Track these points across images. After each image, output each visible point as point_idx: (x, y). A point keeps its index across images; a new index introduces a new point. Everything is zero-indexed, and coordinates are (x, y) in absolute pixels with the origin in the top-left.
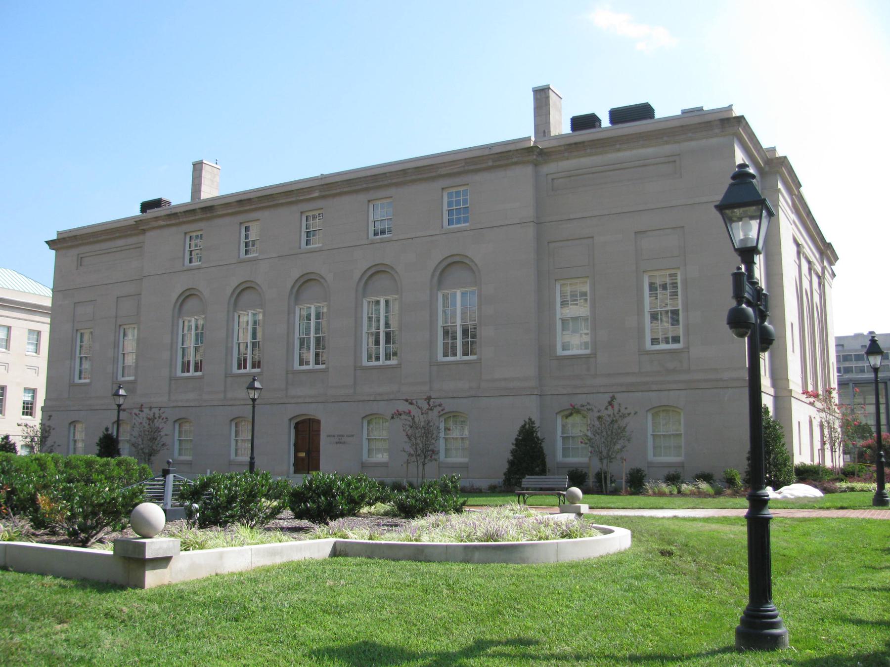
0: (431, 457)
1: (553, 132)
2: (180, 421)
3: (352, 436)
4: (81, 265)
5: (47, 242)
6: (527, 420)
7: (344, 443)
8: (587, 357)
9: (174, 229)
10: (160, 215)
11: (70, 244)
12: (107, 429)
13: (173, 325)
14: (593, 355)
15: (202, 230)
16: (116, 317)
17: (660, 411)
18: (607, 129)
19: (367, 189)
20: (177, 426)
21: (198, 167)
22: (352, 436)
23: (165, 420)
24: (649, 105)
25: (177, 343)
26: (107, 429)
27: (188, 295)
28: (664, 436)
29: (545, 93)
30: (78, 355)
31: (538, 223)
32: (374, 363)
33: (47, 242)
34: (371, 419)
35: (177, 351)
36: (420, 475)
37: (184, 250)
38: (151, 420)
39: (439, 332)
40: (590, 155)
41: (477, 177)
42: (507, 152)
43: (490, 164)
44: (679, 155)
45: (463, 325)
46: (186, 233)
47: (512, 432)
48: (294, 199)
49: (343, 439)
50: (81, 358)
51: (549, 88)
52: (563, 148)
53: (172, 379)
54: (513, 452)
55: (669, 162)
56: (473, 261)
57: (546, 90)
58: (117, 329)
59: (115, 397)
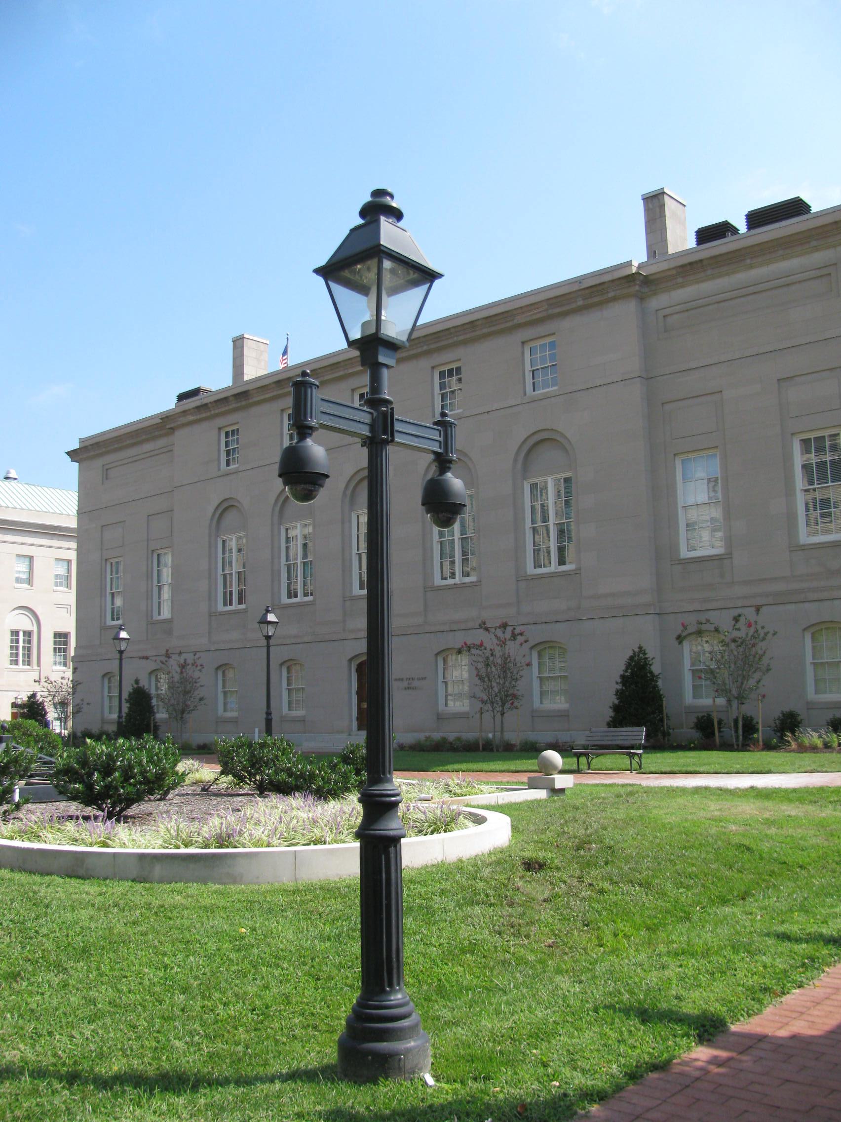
0: (512, 704)
1: (672, 250)
2: (222, 668)
3: (424, 678)
4: (107, 479)
5: (68, 453)
6: (637, 650)
7: (415, 688)
8: (718, 558)
9: (205, 425)
10: (187, 409)
11: (92, 453)
12: (137, 681)
13: (210, 547)
14: (728, 555)
15: (237, 423)
16: (148, 540)
17: (821, 630)
18: (744, 237)
19: (428, 353)
20: (284, 670)
21: (238, 343)
22: (424, 678)
23: (199, 667)
24: (801, 200)
25: (216, 568)
26: (137, 681)
27: (226, 507)
28: (829, 664)
29: (659, 200)
30: (108, 590)
31: (648, 378)
32: (229, 608)
33: (68, 453)
34: (447, 656)
35: (216, 579)
36: (498, 728)
37: (219, 451)
38: (183, 666)
39: (527, 535)
40: (713, 277)
41: (566, 324)
42: (600, 284)
43: (580, 303)
44: (836, 264)
45: (557, 524)
46: (220, 429)
47: (617, 666)
48: (341, 373)
49: (415, 683)
50: (113, 594)
51: (664, 193)
52: (674, 272)
53: (213, 615)
54: (619, 694)
55: (821, 276)
56: (566, 438)
57: (660, 197)
58: (150, 556)
59: (262, 625)
